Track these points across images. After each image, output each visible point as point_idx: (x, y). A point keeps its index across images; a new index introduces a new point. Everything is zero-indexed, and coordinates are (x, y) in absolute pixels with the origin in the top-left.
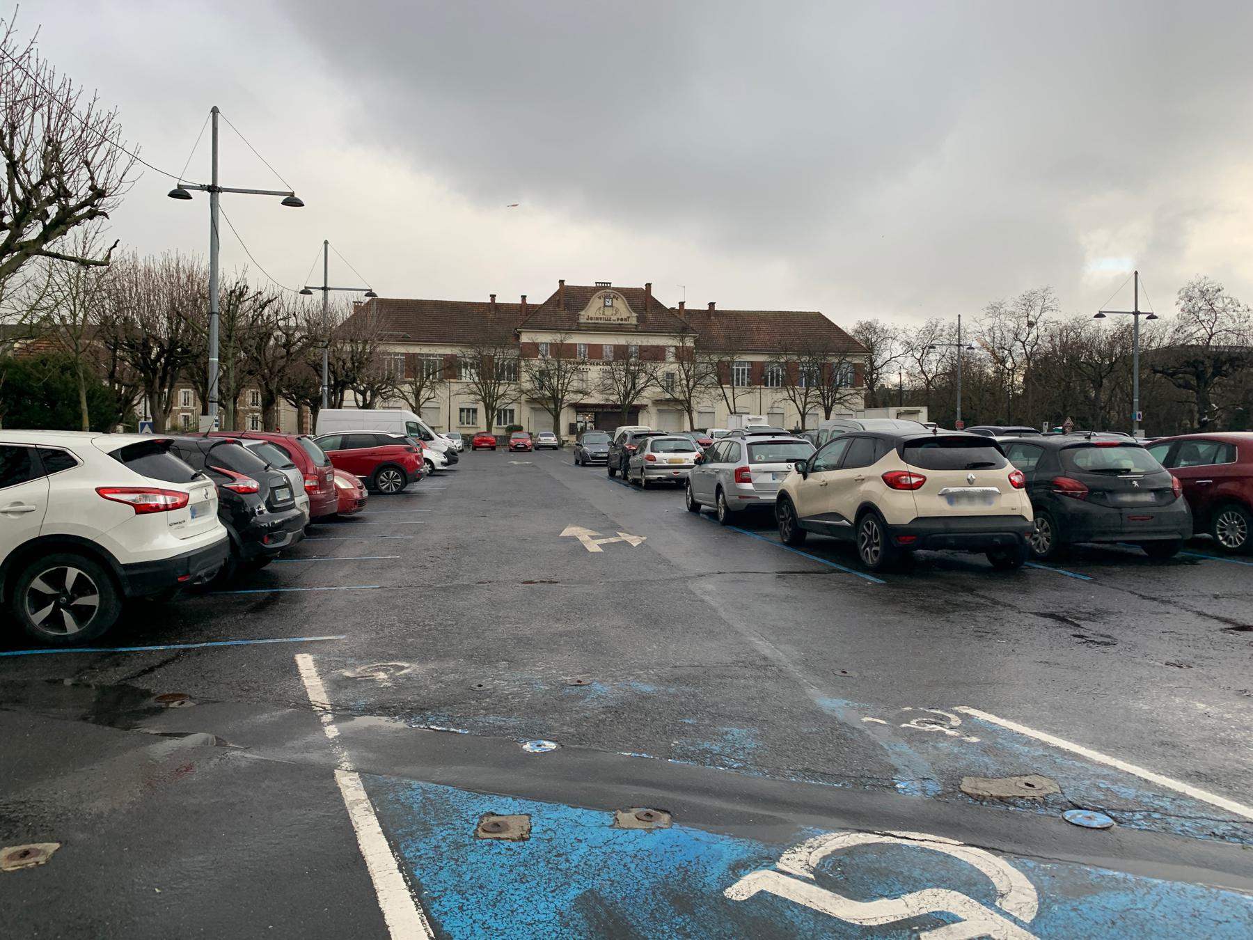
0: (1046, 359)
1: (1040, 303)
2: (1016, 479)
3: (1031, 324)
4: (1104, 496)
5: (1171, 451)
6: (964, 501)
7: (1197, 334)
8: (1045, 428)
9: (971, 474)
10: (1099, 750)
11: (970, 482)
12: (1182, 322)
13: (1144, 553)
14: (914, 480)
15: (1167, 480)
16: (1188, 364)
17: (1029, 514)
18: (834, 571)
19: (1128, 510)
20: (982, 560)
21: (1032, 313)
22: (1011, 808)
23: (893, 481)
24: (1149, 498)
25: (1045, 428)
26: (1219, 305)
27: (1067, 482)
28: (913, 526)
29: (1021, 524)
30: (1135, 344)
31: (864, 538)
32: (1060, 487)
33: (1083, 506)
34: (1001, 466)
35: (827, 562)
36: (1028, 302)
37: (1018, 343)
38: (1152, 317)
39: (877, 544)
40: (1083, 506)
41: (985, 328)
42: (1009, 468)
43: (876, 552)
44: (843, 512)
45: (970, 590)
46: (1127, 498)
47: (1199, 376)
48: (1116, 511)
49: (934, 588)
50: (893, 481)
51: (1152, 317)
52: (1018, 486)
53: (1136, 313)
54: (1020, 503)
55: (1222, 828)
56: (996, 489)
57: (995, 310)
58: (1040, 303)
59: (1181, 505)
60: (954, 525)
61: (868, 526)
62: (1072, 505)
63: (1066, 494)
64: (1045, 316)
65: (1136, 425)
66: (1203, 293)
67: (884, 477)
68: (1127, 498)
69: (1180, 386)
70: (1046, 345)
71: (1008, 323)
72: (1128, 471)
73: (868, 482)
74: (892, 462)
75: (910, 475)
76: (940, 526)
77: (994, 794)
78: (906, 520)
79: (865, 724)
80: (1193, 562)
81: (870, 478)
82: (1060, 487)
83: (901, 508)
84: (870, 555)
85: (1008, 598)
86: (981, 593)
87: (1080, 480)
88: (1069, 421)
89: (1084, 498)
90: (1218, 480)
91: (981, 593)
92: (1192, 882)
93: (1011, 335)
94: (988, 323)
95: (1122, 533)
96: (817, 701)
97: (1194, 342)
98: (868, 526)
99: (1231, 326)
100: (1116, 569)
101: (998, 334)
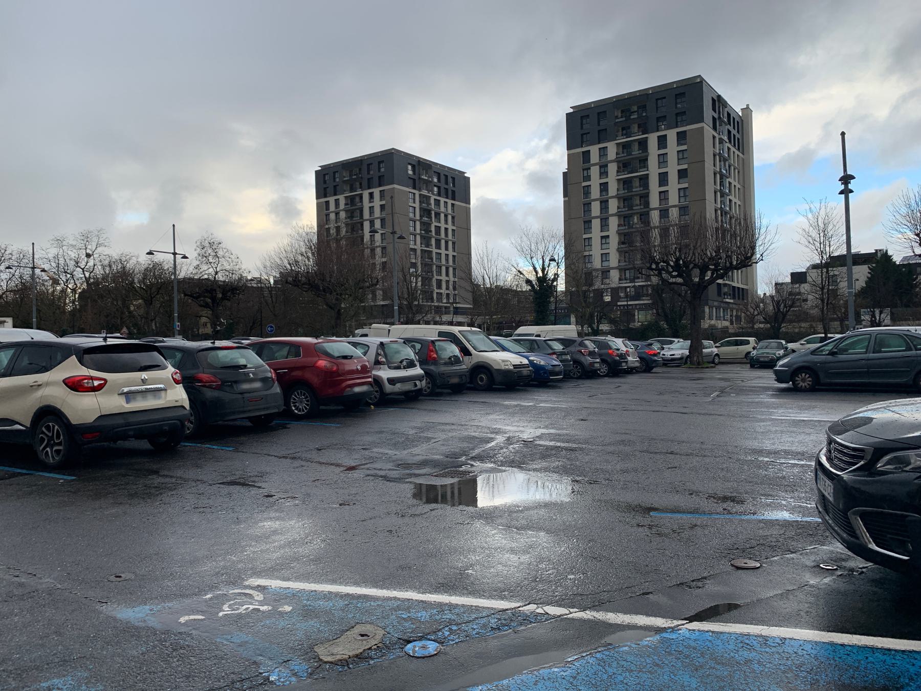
0: (97, 283)
1: (95, 239)
2: (178, 377)
3: (88, 256)
4: (231, 386)
5: (14, 354)
6: (139, 397)
7: (207, 272)
8: (866, 318)
9: (144, 375)
10: (376, 587)
11: (144, 382)
12: (198, 263)
13: (249, 424)
14: (96, 383)
15: (266, 371)
16: (207, 291)
17: (187, 404)
18: (14, 475)
19: (248, 395)
20: (145, 445)
21: (89, 247)
22: (372, 662)
23: (75, 385)
24: (258, 385)
25: (866, 318)
26: (220, 253)
27: (204, 376)
28: (97, 424)
29: (181, 412)
30: (175, 273)
31: (42, 440)
32: (201, 381)
33: (216, 394)
34: (165, 368)
35: (7, 468)
36: (86, 238)
37: (78, 269)
38: (185, 257)
39: (60, 444)
40: (216, 394)
41: (51, 256)
42: (171, 369)
43: (58, 452)
44: (17, 418)
45: (156, 472)
46: (246, 386)
47: (214, 299)
48: (240, 396)
49: (124, 476)
50: (75, 385)
51: (185, 257)
52: (177, 382)
53: (175, 254)
54: (178, 395)
55: (493, 622)
56: (162, 386)
57: (59, 242)
58: (95, 239)
59: (277, 389)
60: (132, 419)
61: (48, 428)
62: (209, 394)
63: (204, 386)
64: (99, 250)
65: (176, 332)
66: (211, 244)
67: (64, 381)
68: (246, 386)
69: (201, 306)
70: (99, 271)
71: (70, 253)
72: (245, 366)
73: (50, 387)
74: (72, 368)
75: (92, 378)
76: (120, 421)
77: (351, 654)
78: (90, 418)
79: (186, 624)
80: (284, 427)
81: (47, 384)
82: (201, 381)
83: (84, 408)
84: (50, 455)
85: (191, 473)
86: (166, 473)
87: (214, 375)
88: (125, 330)
89: (218, 388)
90: (291, 369)
91: (166, 473)
92: (520, 672)
93: (73, 263)
94: (53, 252)
95: (244, 412)
96: (119, 616)
97: (206, 276)
98: (48, 428)
99: (228, 268)
100: (243, 438)
101: (62, 262)
